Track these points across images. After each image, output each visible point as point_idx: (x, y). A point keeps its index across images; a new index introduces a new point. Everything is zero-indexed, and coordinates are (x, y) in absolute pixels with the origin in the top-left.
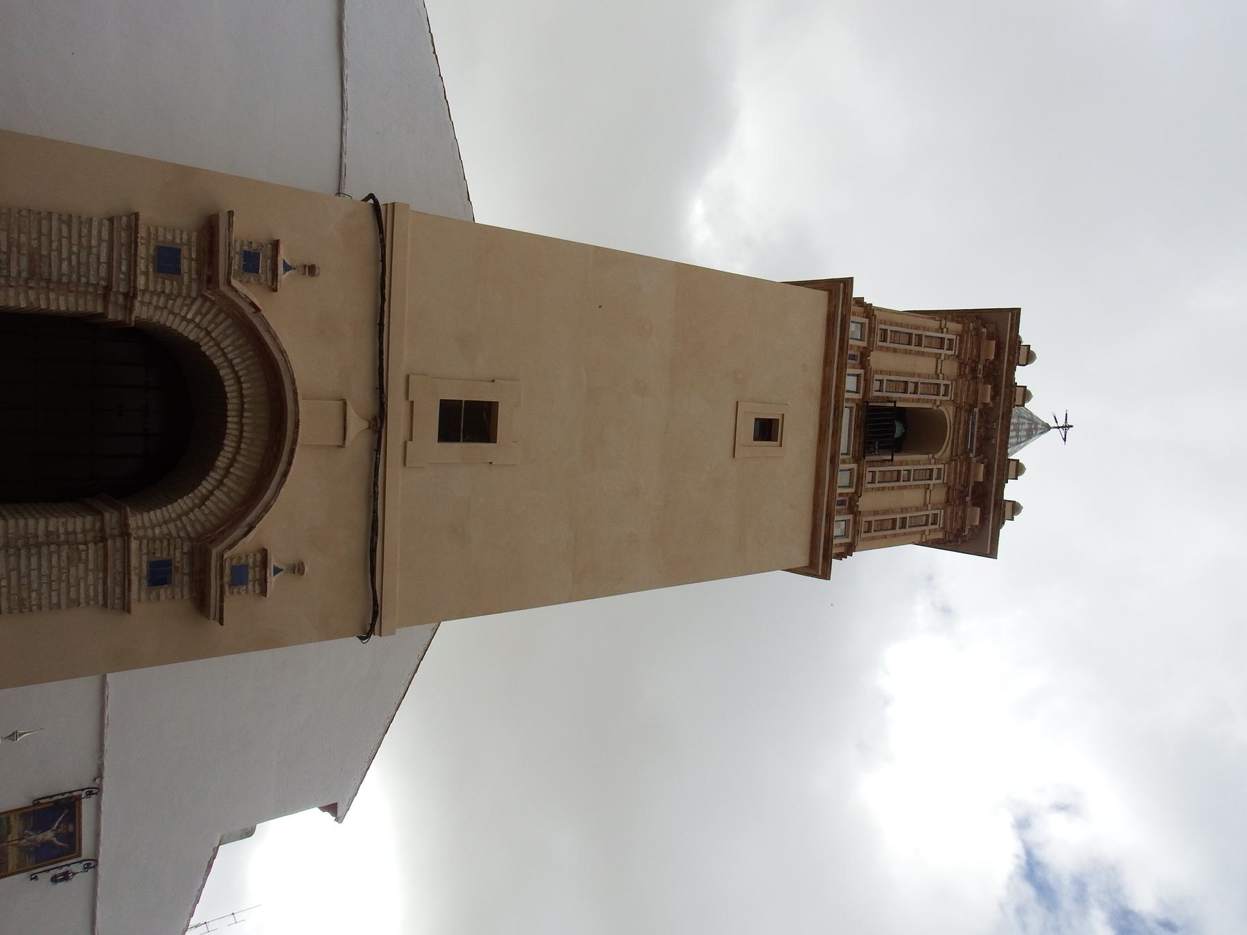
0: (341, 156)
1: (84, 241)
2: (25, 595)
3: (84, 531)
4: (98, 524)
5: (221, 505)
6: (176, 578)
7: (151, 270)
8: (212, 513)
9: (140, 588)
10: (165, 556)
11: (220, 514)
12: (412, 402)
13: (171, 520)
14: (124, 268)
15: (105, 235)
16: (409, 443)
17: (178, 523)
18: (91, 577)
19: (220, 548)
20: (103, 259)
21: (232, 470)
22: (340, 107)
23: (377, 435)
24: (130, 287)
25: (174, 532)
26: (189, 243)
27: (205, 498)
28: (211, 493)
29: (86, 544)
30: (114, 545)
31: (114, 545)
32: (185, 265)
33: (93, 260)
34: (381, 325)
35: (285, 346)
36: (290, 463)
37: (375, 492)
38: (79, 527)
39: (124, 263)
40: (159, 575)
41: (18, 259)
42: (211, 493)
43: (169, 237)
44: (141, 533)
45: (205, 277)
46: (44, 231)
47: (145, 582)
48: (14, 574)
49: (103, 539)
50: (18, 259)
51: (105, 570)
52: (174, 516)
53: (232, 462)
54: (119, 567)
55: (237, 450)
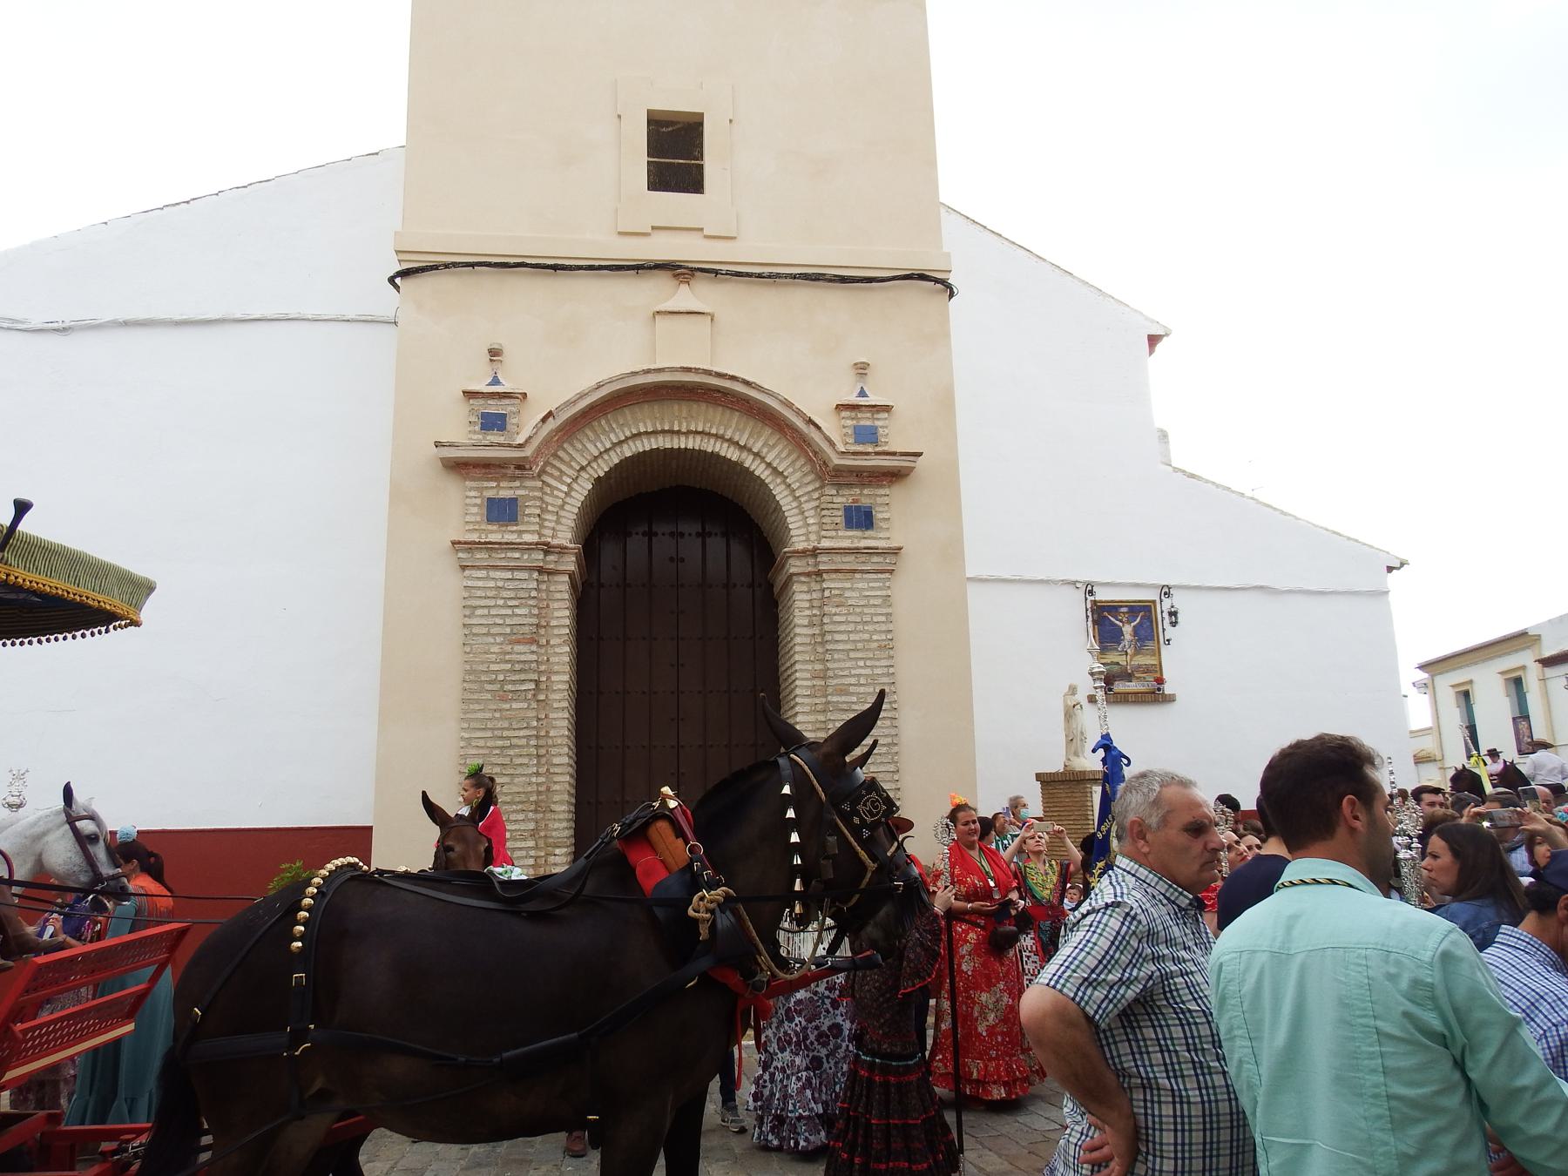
6: (865, 502)
7: (515, 528)
12: (653, 228)
14: (517, 555)
20: (508, 575)
22: (716, 240)
30: (825, 562)
31: (825, 562)
32: (505, 494)
34: (555, 268)
39: (509, 555)
44: (813, 537)
45: (517, 472)
47: (868, 533)
48: (852, 655)
52: (795, 504)
53: (732, 442)
54: (851, 558)
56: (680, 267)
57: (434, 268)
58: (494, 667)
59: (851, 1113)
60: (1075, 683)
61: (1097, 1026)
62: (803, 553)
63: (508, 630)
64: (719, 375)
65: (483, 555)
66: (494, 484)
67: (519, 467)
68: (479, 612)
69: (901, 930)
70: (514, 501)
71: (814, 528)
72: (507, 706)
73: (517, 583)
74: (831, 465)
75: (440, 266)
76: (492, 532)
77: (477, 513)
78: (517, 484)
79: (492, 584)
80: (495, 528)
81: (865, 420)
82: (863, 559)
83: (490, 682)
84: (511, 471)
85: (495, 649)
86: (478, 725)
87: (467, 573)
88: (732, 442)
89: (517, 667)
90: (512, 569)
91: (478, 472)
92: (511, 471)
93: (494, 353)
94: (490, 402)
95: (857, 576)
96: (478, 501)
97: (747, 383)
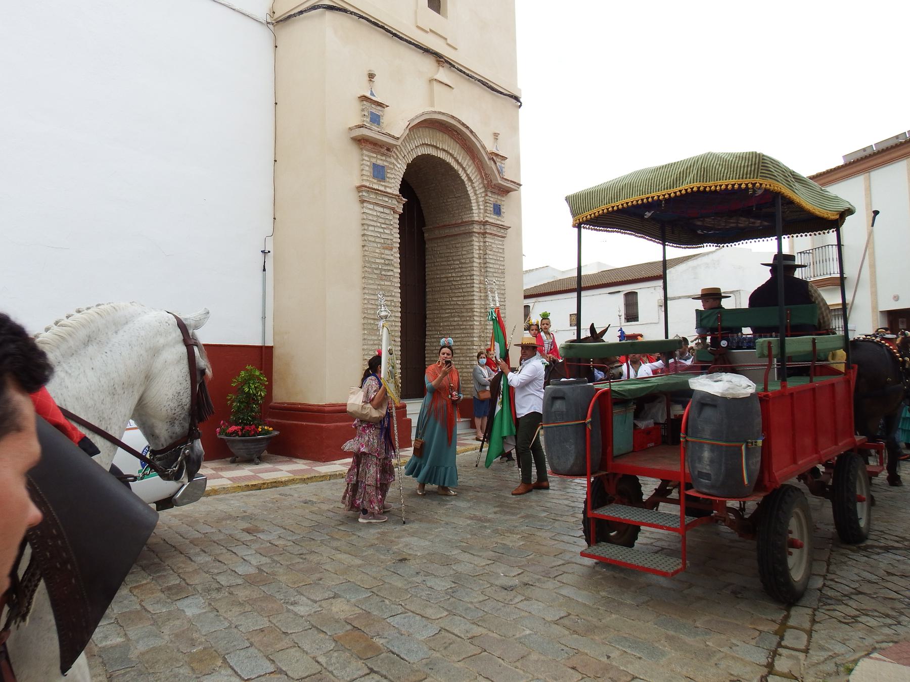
0: (234, 10)
1: (375, 219)
2: (500, 271)
3: (479, 242)
4: (477, 235)
5: (473, 172)
6: (499, 203)
7: (383, 184)
8: (476, 177)
9: (500, 221)
10: (492, 206)
11: (476, 173)
12: (431, 30)
13: (477, 198)
14: (387, 200)
15: (371, 206)
16: (449, 42)
17: (479, 196)
18: (497, 242)
19: (499, 178)
20: (381, 210)
21: (460, 161)
22: (439, 37)
23: (446, 64)
24: (395, 198)
25: (482, 199)
26: (370, 157)
27: (470, 179)
28: (467, 175)
29: (485, 242)
30: (489, 229)
31: (489, 229)
32: (379, 162)
33: (383, 215)
34: (395, 35)
35: (420, 112)
36: (467, 127)
37: (468, 75)
38: (477, 244)
39: (384, 199)
40: (498, 210)
41: (387, 255)
42: (467, 175)
43: (367, 168)
44: (482, 215)
45: (386, 151)
46: (373, 240)
47: (500, 218)
48: (495, 275)
49: (486, 233)
50: (387, 255)
51: (495, 235)
52: (475, 197)
53: (457, 161)
54: (495, 229)
55: (451, 155)
56: (442, 58)
57: (345, 11)
58: (378, 261)
59: (689, 363)
60: (896, 294)
61: (732, 333)
62: (480, 223)
63: (382, 241)
64: (463, 124)
65: (372, 196)
66: (375, 156)
67: (388, 150)
68: (371, 228)
69: (64, 554)
70: (383, 167)
71: (482, 211)
72: (383, 283)
73: (385, 215)
74: (494, 182)
75: (349, 11)
76: (375, 183)
77: (368, 171)
78: (384, 158)
79: (375, 213)
80: (375, 181)
81: (376, 110)
82: (499, 230)
83: (376, 269)
84: (384, 150)
85: (377, 251)
86: (371, 292)
87: (365, 204)
88: (457, 161)
89: (387, 262)
90: (384, 207)
91: (370, 146)
92: (384, 150)
93: (371, 76)
94: (373, 106)
95: (496, 237)
96: (369, 163)
97: (471, 132)
